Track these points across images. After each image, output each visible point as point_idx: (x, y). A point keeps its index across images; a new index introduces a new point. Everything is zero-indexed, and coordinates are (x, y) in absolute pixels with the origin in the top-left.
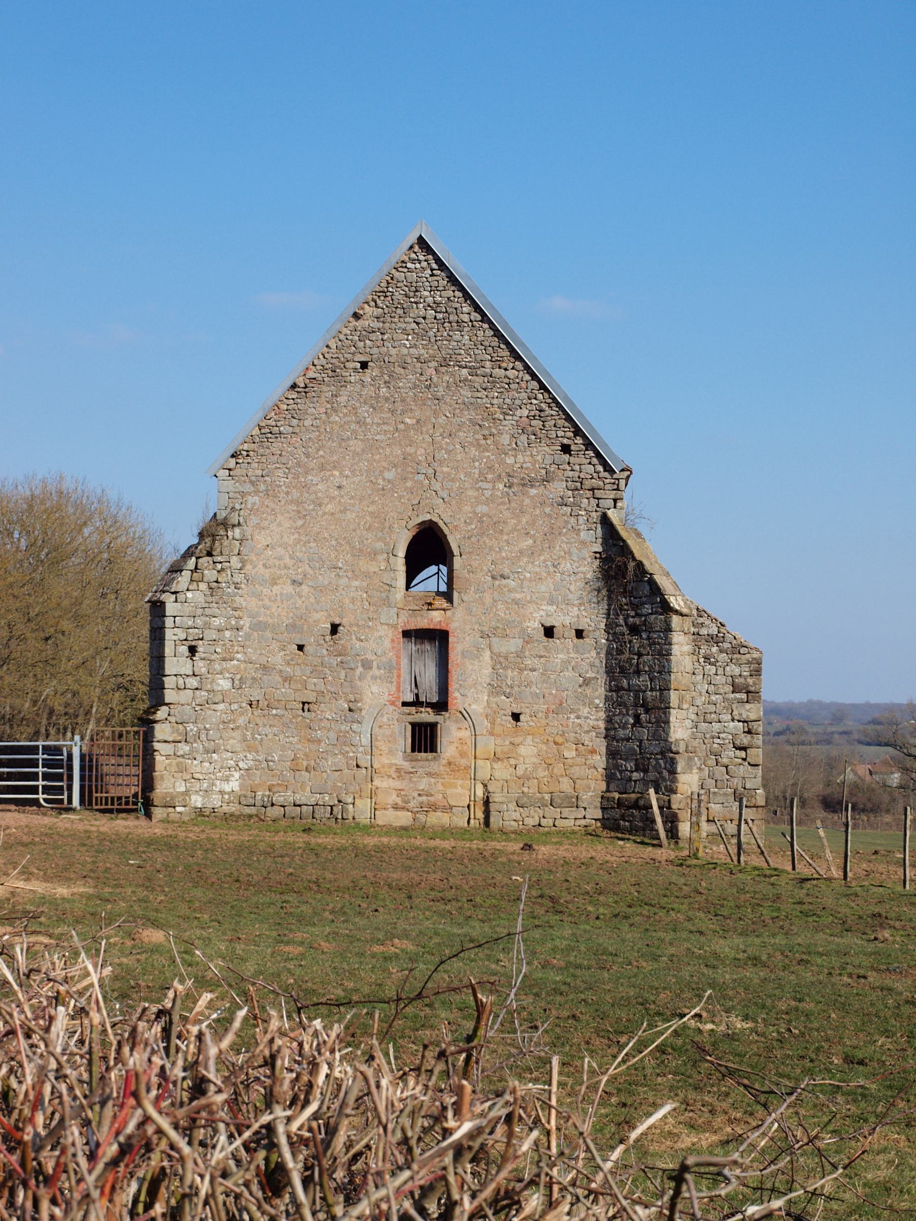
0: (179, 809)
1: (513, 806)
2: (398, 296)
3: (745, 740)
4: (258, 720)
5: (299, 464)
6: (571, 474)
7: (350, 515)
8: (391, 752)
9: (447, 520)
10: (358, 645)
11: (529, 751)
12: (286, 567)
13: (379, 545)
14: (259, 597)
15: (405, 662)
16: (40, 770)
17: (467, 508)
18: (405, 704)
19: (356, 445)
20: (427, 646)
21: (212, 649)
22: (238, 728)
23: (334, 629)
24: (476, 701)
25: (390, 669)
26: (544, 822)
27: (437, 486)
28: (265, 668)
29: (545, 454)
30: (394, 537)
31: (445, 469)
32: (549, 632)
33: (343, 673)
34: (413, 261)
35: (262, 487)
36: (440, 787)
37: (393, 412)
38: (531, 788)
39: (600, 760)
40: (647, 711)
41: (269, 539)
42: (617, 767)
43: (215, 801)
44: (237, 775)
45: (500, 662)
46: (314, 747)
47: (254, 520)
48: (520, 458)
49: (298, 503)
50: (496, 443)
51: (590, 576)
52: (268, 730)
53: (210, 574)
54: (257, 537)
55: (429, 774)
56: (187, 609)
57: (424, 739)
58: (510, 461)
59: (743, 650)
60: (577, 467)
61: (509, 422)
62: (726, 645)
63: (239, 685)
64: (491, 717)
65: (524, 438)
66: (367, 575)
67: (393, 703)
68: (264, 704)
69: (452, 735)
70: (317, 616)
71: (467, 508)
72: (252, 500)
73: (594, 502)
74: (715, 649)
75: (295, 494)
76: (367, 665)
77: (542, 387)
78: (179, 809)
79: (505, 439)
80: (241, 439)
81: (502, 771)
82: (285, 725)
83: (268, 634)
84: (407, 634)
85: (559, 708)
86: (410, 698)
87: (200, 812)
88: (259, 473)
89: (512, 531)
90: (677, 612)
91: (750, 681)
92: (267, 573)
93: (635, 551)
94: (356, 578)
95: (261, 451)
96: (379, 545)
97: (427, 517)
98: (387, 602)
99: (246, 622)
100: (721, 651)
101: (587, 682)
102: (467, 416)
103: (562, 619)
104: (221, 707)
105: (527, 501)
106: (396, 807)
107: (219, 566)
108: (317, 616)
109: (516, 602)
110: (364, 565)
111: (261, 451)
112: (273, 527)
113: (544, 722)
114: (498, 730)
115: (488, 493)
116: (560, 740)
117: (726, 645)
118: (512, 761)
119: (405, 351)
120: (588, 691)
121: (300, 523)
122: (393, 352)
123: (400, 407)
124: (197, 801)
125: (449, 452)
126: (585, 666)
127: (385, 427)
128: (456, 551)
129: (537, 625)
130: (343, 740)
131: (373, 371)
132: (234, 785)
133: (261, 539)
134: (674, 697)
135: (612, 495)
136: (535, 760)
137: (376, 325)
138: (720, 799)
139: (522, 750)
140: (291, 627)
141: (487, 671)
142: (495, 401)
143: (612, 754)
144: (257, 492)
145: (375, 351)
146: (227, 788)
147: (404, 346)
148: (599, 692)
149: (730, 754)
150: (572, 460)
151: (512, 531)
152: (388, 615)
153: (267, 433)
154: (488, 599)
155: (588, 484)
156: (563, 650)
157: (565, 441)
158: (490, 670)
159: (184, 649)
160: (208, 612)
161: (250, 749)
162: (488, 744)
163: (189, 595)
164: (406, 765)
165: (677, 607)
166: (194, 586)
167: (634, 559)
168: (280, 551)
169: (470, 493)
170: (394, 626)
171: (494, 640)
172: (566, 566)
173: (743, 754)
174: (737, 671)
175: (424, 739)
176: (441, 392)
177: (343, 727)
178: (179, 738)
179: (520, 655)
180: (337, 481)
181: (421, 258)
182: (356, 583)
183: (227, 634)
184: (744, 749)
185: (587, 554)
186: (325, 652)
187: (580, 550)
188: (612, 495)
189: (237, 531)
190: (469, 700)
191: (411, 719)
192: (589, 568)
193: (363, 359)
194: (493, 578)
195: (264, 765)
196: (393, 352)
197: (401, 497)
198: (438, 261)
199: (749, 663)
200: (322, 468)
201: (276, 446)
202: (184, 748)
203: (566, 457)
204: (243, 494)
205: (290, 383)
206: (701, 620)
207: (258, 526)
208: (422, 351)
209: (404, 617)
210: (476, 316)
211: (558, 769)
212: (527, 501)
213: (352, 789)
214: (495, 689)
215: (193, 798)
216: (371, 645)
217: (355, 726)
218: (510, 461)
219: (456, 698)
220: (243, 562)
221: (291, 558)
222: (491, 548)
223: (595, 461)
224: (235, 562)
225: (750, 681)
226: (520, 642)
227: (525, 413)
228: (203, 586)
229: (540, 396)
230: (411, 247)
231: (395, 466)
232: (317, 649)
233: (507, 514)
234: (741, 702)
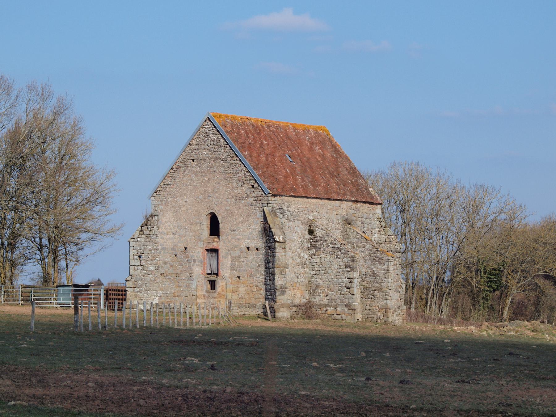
1: (237, 308)
2: (203, 137)
6: (254, 195)
7: (189, 211)
9: (217, 212)
10: (192, 254)
11: (242, 289)
12: (171, 229)
13: (198, 221)
14: (163, 238)
15: (207, 260)
16: (93, 296)
17: (223, 208)
18: (208, 274)
19: (191, 188)
20: (214, 254)
21: (147, 257)
24: (226, 272)
25: (201, 262)
26: (246, 313)
27: (214, 200)
28: (165, 263)
29: (246, 189)
32: (248, 248)
34: (207, 125)
35: (164, 202)
38: (243, 302)
39: (263, 292)
41: (167, 220)
44: (157, 298)
45: (234, 259)
46: (179, 289)
47: (161, 214)
49: (174, 207)
50: (232, 185)
51: (260, 229)
52: (166, 283)
53: (146, 232)
54: (163, 219)
55: (214, 298)
56: (138, 244)
57: (213, 284)
59: (348, 253)
61: (236, 178)
62: (343, 251)
64: (231, 278)
65: (240, 183)
66: (195, 231)
67: (202, 274)
72: (161, 207)
75: (173, 204)
77: (245, 166)
79: (234, 184)
81: (235, 297)
82: (171, 281)
84: (208, 250)
85: (251, 275)
86: (209, 272)
88: (163, 198)
90: (278, 242)
91: (351, 264)
93: (269, 221)
94: (191, 232)
96: (198, 221)
97: (212, 211)
98: (200, 240)
99: (160, 248)
100: (342, 253)
101: (259, 266)
102: (223, 176)
103: (252, 245)
104: (151, 276)
105: (241, 205)
107: (150, 229)
108: (180, 245)
109: (238, 239)
110: (194, 228)
113: (247, 279)
115: (229, 202)
116: (251, 285)
117: (343, 251)
119: (205, 156)
120: (260, 269)
122: (201, 156)
123: (203, 174)
125: (218, 189)
128: (220, 222)
129: (244, 247)
130: (188, 286)
131: (195, 163)
133: (164, 220)
134: (277, 270)
135: (266, 202)
137: (197, 147)
139: (240, 289)
140: (173, 249)
143: (266, 290)
145: (196, 156)
147: (204, 154)
148: (263, 268)
150: (254, 190)
152: (201, 244)
153: (164, 183)
155: (259, 198)
157: (252, 184)
159: (137, 257)
160: (145, 244)
161: (161, 290)
162: (231, 287)
163: (139, 239)
164: (206, 294)
165: (278, 240)
168: (169, 223)
169: (224, 202)
170: (203, 248)
171: (232, 252)
172: (253, 227)
173: (348, 290)
174: (346, 260)
175: (213, 284)
179: (239, 257)
180: (186, 200)
183: (153, 252)
185: (259, 222)
188: (266, 202)
189: (156, 217)
190: (224, 272)
191: (208, 279)
196: (201, 156)
198: (214, 125)
200: (181, 196)
203: (253, 189)
204: (158, 205)
206: (335, 242)
207: (163, 216)
209: (205, 245)
210: (225, 143)
211: (251, 295)
212: (241, 205)
214: (232, 268)
217: (191, 282)
218: (236, 191)
219: (221, 272)
220: (158, 227)
222: (230, 221)
223: (261, 190)
224: (155, 227)
226: (239, 252)
227: (240, 175)
228: (143, 236)
232: (181, 256)
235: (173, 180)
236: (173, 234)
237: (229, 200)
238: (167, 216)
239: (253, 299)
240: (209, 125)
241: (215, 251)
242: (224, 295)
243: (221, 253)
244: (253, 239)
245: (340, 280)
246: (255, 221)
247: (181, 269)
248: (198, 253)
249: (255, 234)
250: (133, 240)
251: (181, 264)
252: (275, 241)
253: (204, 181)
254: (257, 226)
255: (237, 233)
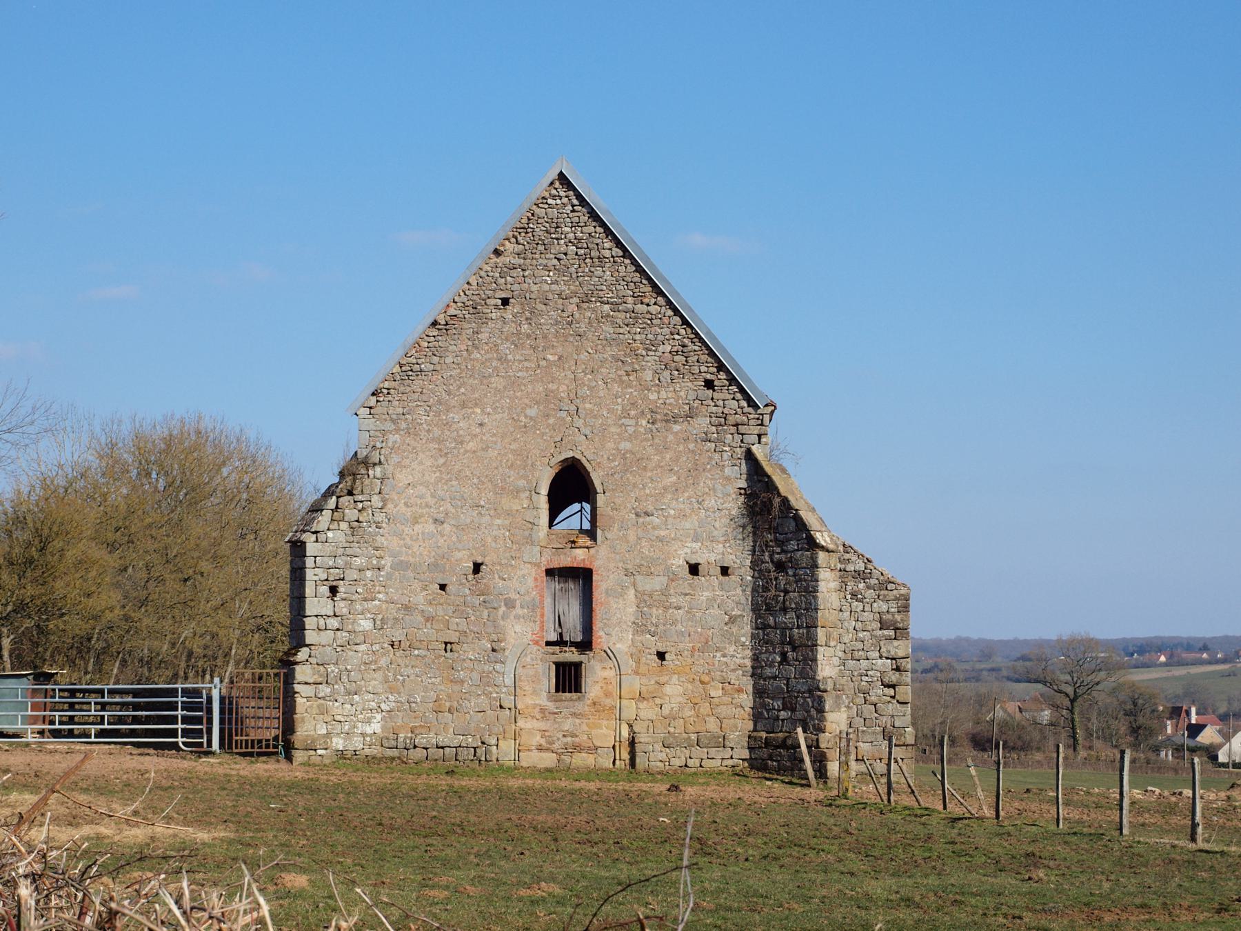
0: (319, 752)
1: (658, 747)
3: (893, 677)
4: (400, 661)
5: (439, 402)
7: (492, 453)
8: (535, 692)
10: (501, 583)
11: (674, 690)
14: (400, 535)
15: (548, 601)
17: (610, 445)
18: (548, 644)
20: (571, 585)
21: (353, 589)
22: (379, 669)
23: (477, 568)
27: (579, 423)
28: (407, 608)
29: (688, 389)
30: (537, 474)
31: (588, 406)
33: (486, 613)
34: (553, 197)
36: (585, 728)
37: (534, 348)
38: (677, 728)
39: (747, 700)
40: (794, 649)
41: (410, 478)
42: (764, 705)
43: (357, 743)
44: (379, 717)
45: (644, 599)
46: (457, 688)
47: (395, 458)
48: (663, 394)
49: (440, 441)
52: (409, 671)
53: (351, 514)
54: (398, 476)
55: (574, 715)
56: (328, 549)
57: (568, 679)
58: (653, 396)
59: (890, 586)
60: (721, 403)
61: (652, 358)
62: (873, 582)
63: (380, 624)
65: (666, 373)
66: (509, 513)
67: (536, 643)
68: (405, 644)
69: (597, 674)
70: (458, 555)
71: (610, 445)
72: (393, 438)
73: (738, 438)
74: (862, 586)
75: (437, 432)
76: (510, 604)
78: (319, 752)
79: (648, 375)
80: (381, 377)
81: (648, 711)
83: (410, 574)
84: (550, 573)
85: (706, 647)
86: (553, 637)
87: (341, 755)
88: (401, 410)
89: (655, 468)
90: (823, 548)
91: (898, 617)
92: (408, 512)
95: (402, 389)
96: (522, 483)
97: (570, 454)
98: (530, 541)
99: (387, 562)
100: (868, 587)
101: (732, 620)
102: (610, 352)
103: (708, 556)
104: (362, 647)
105: (671, 437)
106: (540, 749)
108: (458, 555)
109: (660, 539)
110: (507, 503)
111: (402, 389)
112: (415, 465)
113: (689, 661)
114: (643, 669)
115: (631, 430)
116: (706, 678)
117: (873, 582)
118: (658, 701)
119: (546, 287)
120: (734, 629)
121: (441, 461)
122: (534, 288)
124: (338, 743)
126: (730, 604)
127: (527, 364)
129: (681, 562)
130: (486, 680)
132: (376, 727)
133: (403, 478)
135: (756, 430)
136: (680, 699)
138: (868, 738)
139: (668, 690)
140: (434, 566)
141: (632, 609)
142: (638, 337)
143: (759, 693)
144: (398, 430)
145: (516, 287)
146: (369, 730)
147: (545, 282)
148: (745, 630)
149: (878, 692)
150: (716, 395)
151: (655, 468)
153: (407, 371)
154: (632, 536)
156: (709, 587)
157: (709, 377)
158: (635, 608)
159: (324, 590)
160: (349, 551)
161: (392, 690)
162: (633, 684)
163: (330, 534)
164: (551, 706)
165: (823, 543)
166: (334, 526)
167: (779, 495)
168: (422, 490)
169: (613, 429)
170: (537, 565)
171: (638, 578)
172: (711, 502)
173: (891, 692)
174: (884, 607)
175: (568, 679)
176: (583, 327)
177: (486, 668)
178: (320, 680)
179: (665, 592)
181: (562, 194)
182: (499, 522)
183: (369, 574)
184: (893, 686)
185: (732, 490)
186: (467, 592)
187: (724, 486)
188: (756, 430)
189: (378, 469)
190: (613, 639)
192: (733, 505)
193: (504, 296)
194: (637, 515)
195: (406, 706)
196: (534, 288)
197: (543, 434)
199: (896, 599)
200: (464, 405)
201: (417, 383)
202: (325, 690)
204: (384, 433)
205: (431, 320)
206: (847, 556)
208: (564, 288)
211: (705, 709)
212: (671, 437)
213: (495, 730)
214: (640, 627)
215: (335, 740)
216: (514, 584)
217: (498, 667)
218: (653, 396)
220: (385, 501)
221: (433, 496)
222: (635, 485)
223: (739, 396)
225: (898, 617)
226: (665, 580)
227: (668, 348)
228: (344, 526)
229: (683, 332)
230: (552, 183)
231: (537, 403)
232: (460, 588)
233: (650, 450)
234: (889, 639)
235: (436, 359)
236: (436, 521)
237: (632, 422)
238: (415, 465)
239: (712, 719)
240: (563, 202)
241: (582, 577)
242: (612, 708)
243: (601, 585)
244: (713, 540)
245: (864, 663)
246: (719, 487)
247: (463, 626)
248: (523, 578)
249: (717, 525)
250: (313, 537)
251: (459, 611)
252: (812, 544)
253: (543, 363)
254: (725, 494)
255: (656, 520)
